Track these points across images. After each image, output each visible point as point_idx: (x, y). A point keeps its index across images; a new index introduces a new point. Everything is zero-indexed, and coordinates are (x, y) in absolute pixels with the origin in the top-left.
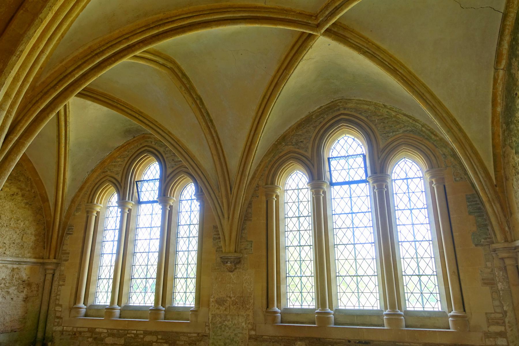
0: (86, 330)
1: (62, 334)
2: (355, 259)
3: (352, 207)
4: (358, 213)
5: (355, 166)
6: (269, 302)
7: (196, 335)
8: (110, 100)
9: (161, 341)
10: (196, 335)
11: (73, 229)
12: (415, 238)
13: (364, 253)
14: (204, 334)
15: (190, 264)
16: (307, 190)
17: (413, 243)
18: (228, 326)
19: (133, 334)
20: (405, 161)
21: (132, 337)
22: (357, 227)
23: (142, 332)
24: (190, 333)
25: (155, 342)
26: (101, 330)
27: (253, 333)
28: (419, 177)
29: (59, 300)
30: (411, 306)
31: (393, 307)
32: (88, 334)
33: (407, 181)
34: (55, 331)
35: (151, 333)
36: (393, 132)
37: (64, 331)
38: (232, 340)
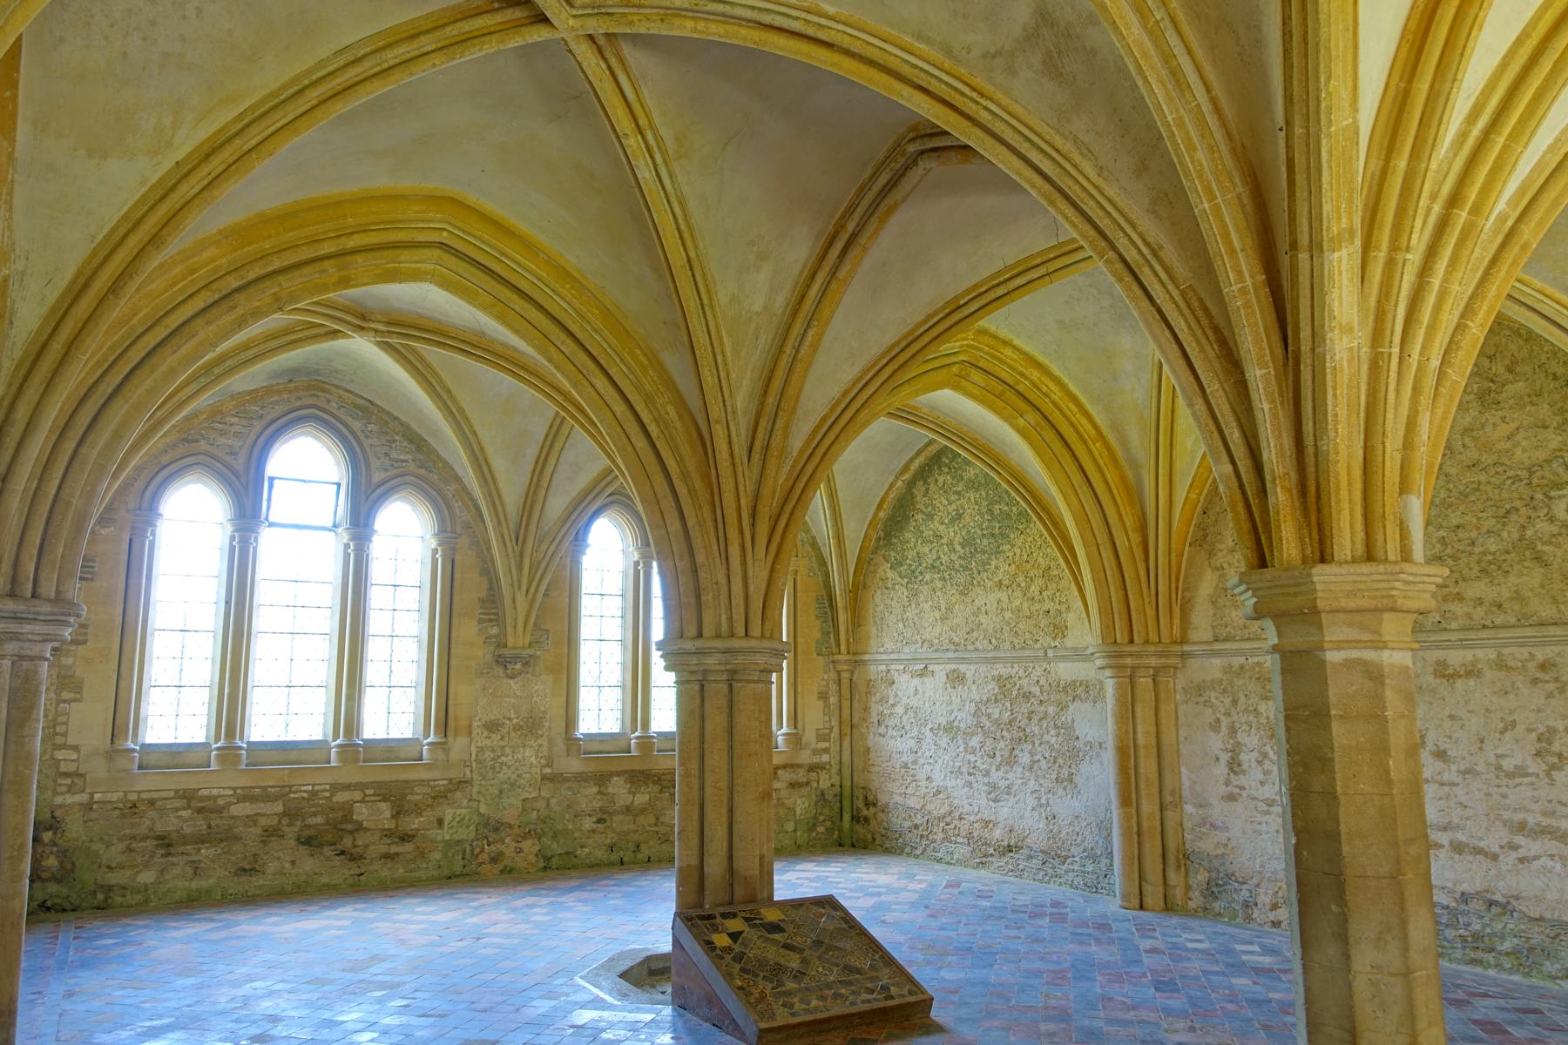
0: (172, 794)
9: (372, 798)
21: (303, 798)
23: (328, 787)
26: (215, 792)
27: (548, 770)
32: (177, 803)
34: (60, 806)
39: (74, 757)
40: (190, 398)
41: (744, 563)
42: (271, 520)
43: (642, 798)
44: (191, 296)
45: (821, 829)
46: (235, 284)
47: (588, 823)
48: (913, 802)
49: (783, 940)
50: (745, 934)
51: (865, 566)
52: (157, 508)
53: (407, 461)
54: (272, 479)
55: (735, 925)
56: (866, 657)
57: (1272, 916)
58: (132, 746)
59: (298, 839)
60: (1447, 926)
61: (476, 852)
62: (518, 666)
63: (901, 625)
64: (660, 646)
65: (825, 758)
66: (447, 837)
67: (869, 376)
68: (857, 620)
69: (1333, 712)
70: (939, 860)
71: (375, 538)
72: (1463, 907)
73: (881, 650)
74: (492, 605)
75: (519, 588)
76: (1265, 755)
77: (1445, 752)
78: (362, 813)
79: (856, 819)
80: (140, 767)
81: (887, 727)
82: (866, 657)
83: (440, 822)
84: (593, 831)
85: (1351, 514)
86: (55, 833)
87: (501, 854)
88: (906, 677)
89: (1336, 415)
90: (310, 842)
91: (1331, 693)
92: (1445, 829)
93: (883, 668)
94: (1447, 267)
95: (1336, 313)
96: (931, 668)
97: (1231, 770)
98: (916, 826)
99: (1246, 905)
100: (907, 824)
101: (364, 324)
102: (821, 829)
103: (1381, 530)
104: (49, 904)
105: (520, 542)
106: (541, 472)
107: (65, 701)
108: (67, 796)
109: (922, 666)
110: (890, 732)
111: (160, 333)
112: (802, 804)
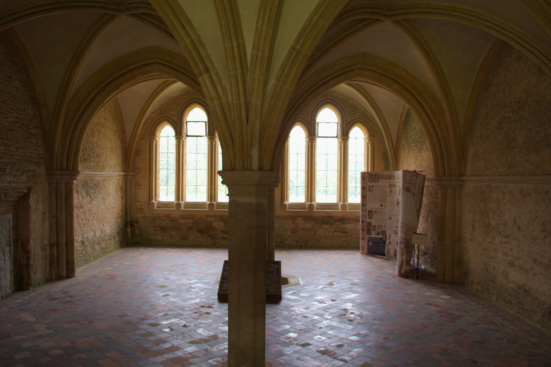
0: (164, 216)
1: (145, 218)
6: (150, 197)
8: (512, 33)
19: (199, 217)
21: (198, 219)
23: (205, 216)
26: (175, 216)
29: (138, 198)
31: (211, 200)
32: (166, 218)
35: (211, 216)
38: (543, 224)
39: (140, 204)
42: (319, 136)
43: (309, 225)
47: (289, 233)
51: (398, 139)
54: (318, 123)
71: (350, 140)
78: (215, 224)
90: (201, 231)
107: (137, 189)
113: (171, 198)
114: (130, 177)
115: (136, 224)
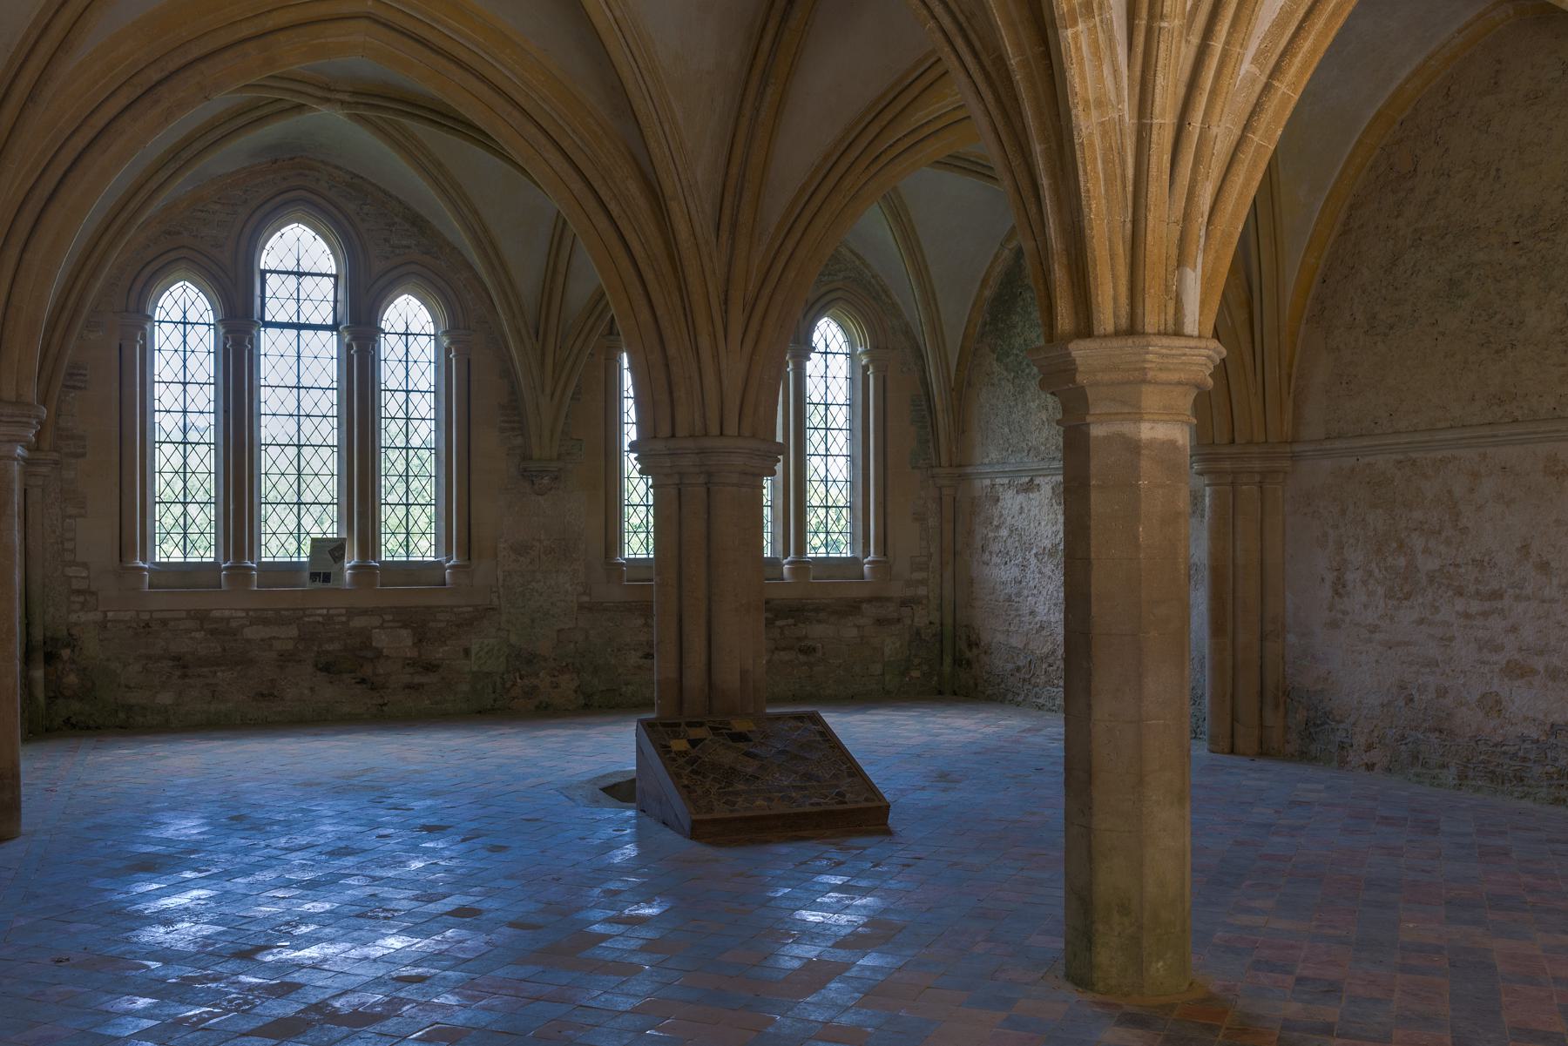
0: (184, 614)
2: (299, 475)
3: (407, 377)
4: (397, 390)
5: (316, 295)
7: (470, 609)
9: (391, 624)
10: (470, 609)
11: (85, 375)
12: (185, 436)
13: (316, 464)
14: (489, 607)
15: (822, 481)
16: (427, 338)
17: (181, 447)
18: (537, 591)
19: (319, 615)
20: (185, 287)
21: (319, 622)
22: (308, 416)
23: (344, 611)
24: (459, 607)
25: (376, 628)
26: (227, 613)
27: (585, 599)
28: (208, 322)
30: (269, 554)
33: (185, 328)
34: (76, 624)
35: (365, 612)
36: (829, 274)
37: (109, 621)
40: (161, 186)
41: (716, 356)
44: (113, 93)
45: (915, 674)
46: (156, 77)
48: (1016, 642)
49: (746, 749)
50: (706, 741)
52: (145, 309)
53: (409, 247)
55: (697, 733)
56: (969, 470)
57: (1366, 758)
58: (141, 564)
59: (316, 666)
60: (1535, 762)
61: (508, 685)
62: (546, 481)
63: (1007, 430)
64: (634, 447)
65: (922, 591)
66: (475, 669)
67: (854, 135)
68: (961, 426)
69: (1093, 482)
70: (1040, 707)
72: (1552, 740)
73: (986, 461)
74: (513, 411)
75: (543, 391)
76: (1371, 574)
77: (1548, 563)
78: (381, 640)
79: (957, 662)
80: (150, 587)
81: (991, 553)
82: (969, 470)
83: (467, 652)
84: (640, 667)
85: (1115, 288)
86: (73, 651)
87: (535, 687)
88: (1010, 493)
89: (1088, 191)
90: (328, 668)
91: (1092, 464)
92: (1541, 653)
93: (987, 482)
94: (1230, 28)
95: (1078, 89)
96: (1036, 482)
97: (1337, 593)
98: (1018, 669)
99: (1342, 747)
100: (1010, 666)
101: (329, 95)
102: (915, 674)
103: (1141, 304)
104: (73, 720)
105: (541, 337)
106: (557, 255)
107: (70, 517)
108: (81, 614)
109: (1027, 479)
110: (995, 559)
111: (88, 133)
112: (891, 644)
113: (204, 551)
114: (44, 470)
115: (66, 653)
